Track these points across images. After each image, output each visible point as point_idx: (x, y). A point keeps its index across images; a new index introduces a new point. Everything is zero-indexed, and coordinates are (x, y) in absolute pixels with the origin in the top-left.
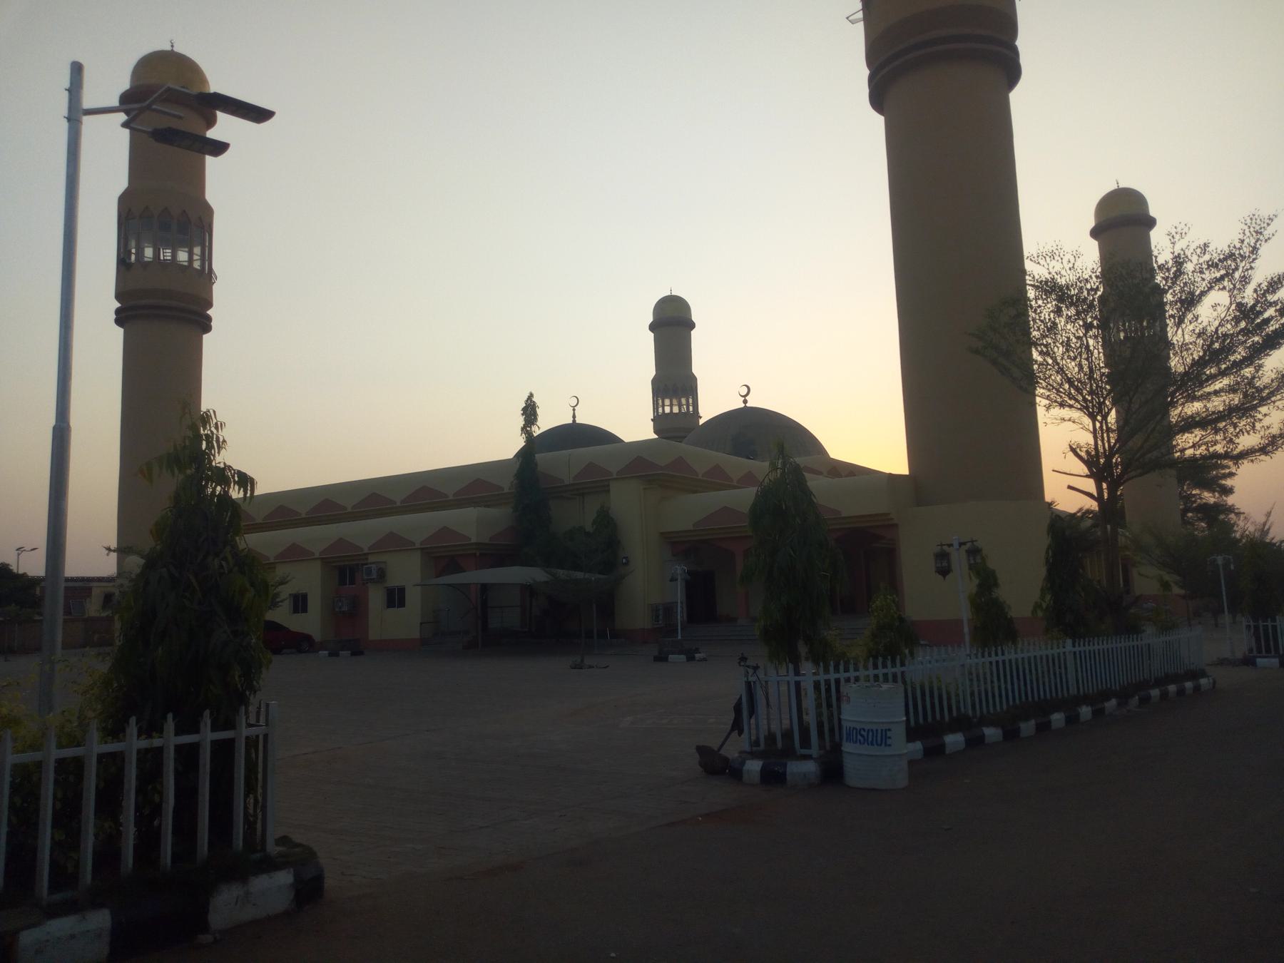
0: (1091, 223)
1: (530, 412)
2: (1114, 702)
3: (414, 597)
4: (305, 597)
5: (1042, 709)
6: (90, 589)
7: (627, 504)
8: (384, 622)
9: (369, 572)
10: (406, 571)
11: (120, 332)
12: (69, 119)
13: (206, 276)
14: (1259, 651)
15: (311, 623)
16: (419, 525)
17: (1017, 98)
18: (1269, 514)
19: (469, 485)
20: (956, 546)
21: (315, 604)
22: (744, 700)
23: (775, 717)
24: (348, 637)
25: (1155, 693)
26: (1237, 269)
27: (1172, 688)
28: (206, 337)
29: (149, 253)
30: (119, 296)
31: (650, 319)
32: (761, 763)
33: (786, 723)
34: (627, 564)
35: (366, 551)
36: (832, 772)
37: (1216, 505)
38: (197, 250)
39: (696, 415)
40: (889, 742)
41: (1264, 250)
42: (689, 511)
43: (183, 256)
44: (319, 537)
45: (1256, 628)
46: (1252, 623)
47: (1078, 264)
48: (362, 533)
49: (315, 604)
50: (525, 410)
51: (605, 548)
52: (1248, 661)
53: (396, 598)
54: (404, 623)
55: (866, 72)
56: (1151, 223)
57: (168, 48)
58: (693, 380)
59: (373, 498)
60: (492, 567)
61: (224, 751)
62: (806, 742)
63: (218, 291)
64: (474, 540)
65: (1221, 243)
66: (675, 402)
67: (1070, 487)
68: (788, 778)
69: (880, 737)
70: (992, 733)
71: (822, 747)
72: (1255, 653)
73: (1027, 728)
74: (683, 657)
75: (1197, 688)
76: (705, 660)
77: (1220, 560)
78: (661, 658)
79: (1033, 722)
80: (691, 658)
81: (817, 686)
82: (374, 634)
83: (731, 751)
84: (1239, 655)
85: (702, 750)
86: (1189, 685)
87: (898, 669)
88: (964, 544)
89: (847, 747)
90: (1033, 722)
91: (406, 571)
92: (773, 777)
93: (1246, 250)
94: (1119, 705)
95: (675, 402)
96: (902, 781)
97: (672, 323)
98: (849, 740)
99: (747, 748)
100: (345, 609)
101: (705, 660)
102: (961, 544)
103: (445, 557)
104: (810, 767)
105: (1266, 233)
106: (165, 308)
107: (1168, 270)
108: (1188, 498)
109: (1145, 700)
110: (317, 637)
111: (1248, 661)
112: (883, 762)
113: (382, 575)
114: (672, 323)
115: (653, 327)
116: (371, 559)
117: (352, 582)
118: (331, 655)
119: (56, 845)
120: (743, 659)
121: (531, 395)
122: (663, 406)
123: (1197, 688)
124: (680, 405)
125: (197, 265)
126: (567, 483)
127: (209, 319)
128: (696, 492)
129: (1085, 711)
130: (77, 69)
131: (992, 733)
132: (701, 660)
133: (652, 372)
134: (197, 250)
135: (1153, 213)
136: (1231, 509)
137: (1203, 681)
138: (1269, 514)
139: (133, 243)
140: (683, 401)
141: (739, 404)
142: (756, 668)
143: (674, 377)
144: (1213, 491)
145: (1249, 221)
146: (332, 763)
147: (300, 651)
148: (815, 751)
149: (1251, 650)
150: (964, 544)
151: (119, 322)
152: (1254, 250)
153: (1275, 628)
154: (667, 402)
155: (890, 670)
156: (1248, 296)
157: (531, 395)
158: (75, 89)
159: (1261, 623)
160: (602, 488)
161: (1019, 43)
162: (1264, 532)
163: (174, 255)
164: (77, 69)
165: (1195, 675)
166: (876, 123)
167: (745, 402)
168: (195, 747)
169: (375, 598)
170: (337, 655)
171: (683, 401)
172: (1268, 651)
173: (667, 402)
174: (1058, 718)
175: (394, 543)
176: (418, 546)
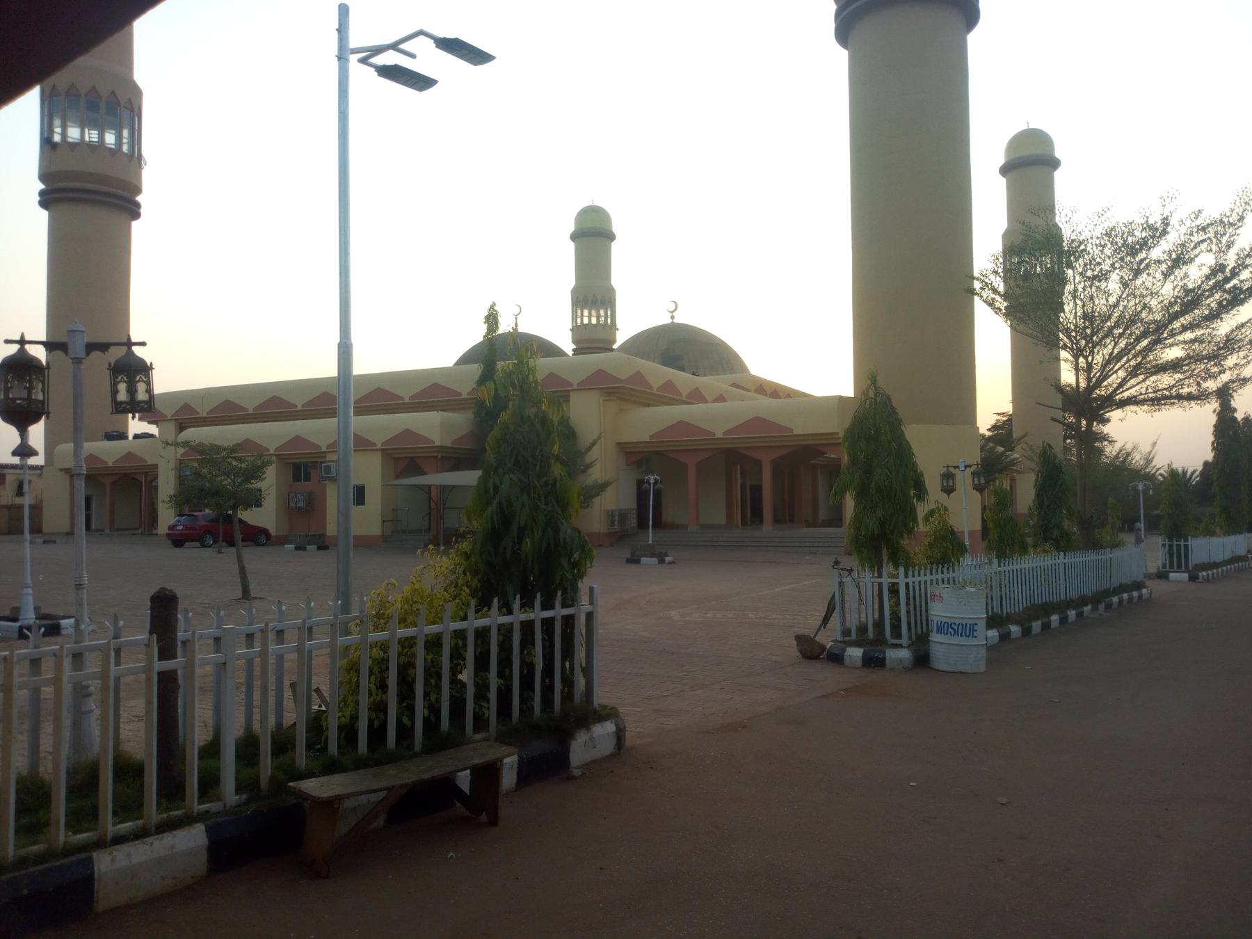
0: (1001, 160)
1: (492, 319)
2: (1089, 607)
5: (1045, 609)
7: (586, 414)
9: (328, 469)
11: (44, 215)
12: (339, 59)
13: (135, 159)
15: (264, 516)
16: (382, 426)
17: (975, 40)
18: (1154, 444)
19: (428, 391)
20: (962, 468)
24: (305, 529)
26: (1225, 234)
27: (1125, 596)
28: (135, 225)
29: (110, 139)
30: (43, 177)
32: (862, 650)
33: (863, 619)
35: (324, 449)
36: (922, 660)
38: (125, 133)
39: (613, 327)
43: (110, 139)
45: (1171, 546)
47: (1075, 219)
48: (319, 431)
50: (487, 318)
52: (1162, 576)
60: (442, 471)
61: (569, 621)
63: (149, 177)
64: (437, 443)
65: (1212, 212)
66: (594, 313)
69: (968, 630)
71: (910, 638)
73: (1036, 626)
74: (654, 560)
75: (1140, 596)
76: (673, 562)
77: (1140, 487)
78: (634, 560)
79: (1040, 622)
80: (662, 561)
81: (907, 584)
83: (827, 639)
84: (1154, 571)
85: (800, 639)
86: (1135, 594)
87: (951, 575)
88: (970, 466)
89: (935, 637)
90: (1040, 622)
91: (368, 471)
92: (873, 661)
93: (1234, 218)
95: (594, 313)
96: (982, 669)
97: (593, 235)
98: (940, 630)
99: (839, 638)
100: (301, 504)
101: (673, 562)
102: (966, 467)
103: (405, 459)
104: (904, 654)
107: (1157, 229)
109: (1109, 606)
110: (273, 531)
111: (1162, 576)
114: (593, 235)
115: (574, 237)
116: (330, 457)
117: (307, 479)
118: (297, 548)
123: (1140, 596)
124: (598, 317)
125: (125, 148)
127: (138, 205)
128: (648, 405)
129: (1072, 614)
130: (344, 11)
131: (1015, 629)
132: (670, 563)
133: (572, 282)
134: (125, 133)
135: (1058, 154)
136: (1105, 438)
137: (1144, 591)
138: (1154, 444)
139: (57, 122)
140: (602, 312)
141: (666, 320)
142: (850, 571)
143: (593, 290)
146: (673, 634)
147: (258, 544)
148: (904, 641)
149: (1164, 566)
150: (970, 466)
152: (1241, 219)
153: (1186, 547)
154: (586, 312)
155: (946, 576)
156: (1231, 259)
157: (492, 307)
158: (342, 30)
162: (1149, 461)
163: (101, 137)
164: (344, 11)
165: (1138, 586)
166: (841, 57)
167: (673, 317)
168: (552, 619)
170: (304, 549)
171: (602, 312)
172: (1179, 566)
173: (586, 312)
174: (1055, 618)
176: (379, 446)
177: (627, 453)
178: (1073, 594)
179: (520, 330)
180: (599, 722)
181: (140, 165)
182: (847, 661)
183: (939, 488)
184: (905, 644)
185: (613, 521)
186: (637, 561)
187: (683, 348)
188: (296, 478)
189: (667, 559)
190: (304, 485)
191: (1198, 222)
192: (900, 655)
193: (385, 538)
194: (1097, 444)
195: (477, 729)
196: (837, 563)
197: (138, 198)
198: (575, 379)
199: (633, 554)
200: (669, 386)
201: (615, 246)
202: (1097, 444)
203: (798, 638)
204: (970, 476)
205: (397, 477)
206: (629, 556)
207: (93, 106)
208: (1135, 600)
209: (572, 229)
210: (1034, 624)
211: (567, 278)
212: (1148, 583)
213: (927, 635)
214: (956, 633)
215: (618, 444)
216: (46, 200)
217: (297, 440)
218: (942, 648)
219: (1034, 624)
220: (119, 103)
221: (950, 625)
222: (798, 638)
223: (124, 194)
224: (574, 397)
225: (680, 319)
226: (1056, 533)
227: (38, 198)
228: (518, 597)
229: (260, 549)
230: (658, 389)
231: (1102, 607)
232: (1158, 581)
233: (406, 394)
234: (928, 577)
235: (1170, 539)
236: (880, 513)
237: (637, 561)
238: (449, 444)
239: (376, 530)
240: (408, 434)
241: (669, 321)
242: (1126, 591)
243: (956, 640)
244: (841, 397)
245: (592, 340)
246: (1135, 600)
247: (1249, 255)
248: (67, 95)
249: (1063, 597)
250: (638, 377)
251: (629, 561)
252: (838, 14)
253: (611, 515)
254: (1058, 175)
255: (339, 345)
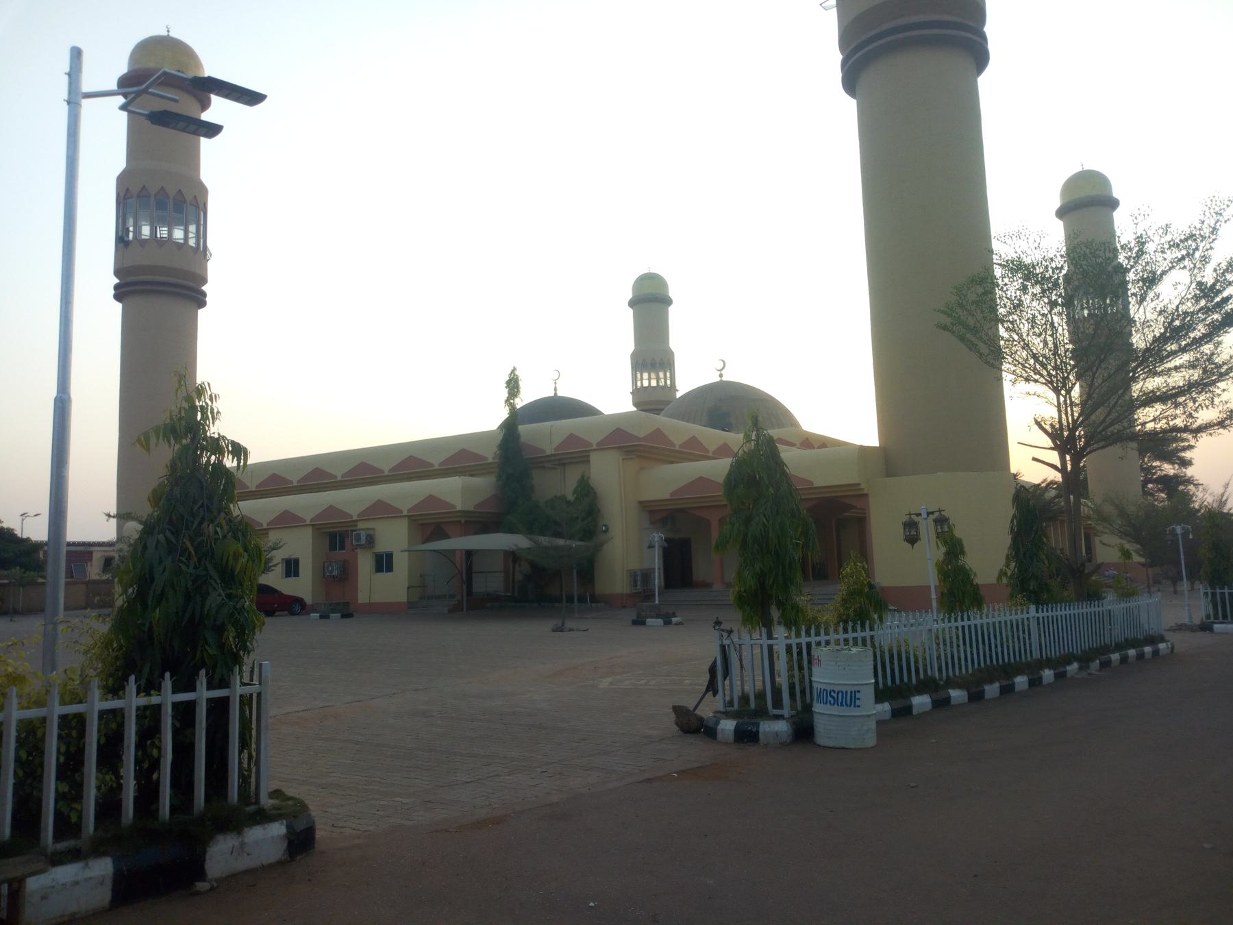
0: (1057, 203)
1: (513, 385)
2: (1075, 665)
3: (401, 563)
4: (297, 562)
6: (91, 553)
7: (606, 472)
8: (372, 586)
9: (358, 538)
10: (394, 537)
11: (118, 306)
12: (69, 102)
13: (201, 253)
14: (1216, 617)
15: (302, 587)
17: (985, 82)
19: (457, 457)
20: (924, 515)
21: (306, 568)
22: (719, 662)
23: (749, 679)
24: (339, 601)
25: (1115, 657)
26: (1197, 249)
27: (1132, 652)
29: (146, 231)
30: (117, 273)
31: (629, 295)
32: (734, 723)
33: (759, 684)
34: (606, 531)
36: (804, 732)
37: (1176, 476)
38: (192, 228)
39: (673, 388)
40: (858, 703)
41: (1223, 230)
42: (666, 481)
44: (308, 504)
45: (1214, 595)
46: (1209, 591)
48: (351, 500)
49: (306, 568)
50: (508, 383)
51: (586, 515)
52: (1206, 627)
53: (384, 563)
54: (393, 587)
55: (839, 57)
56: (1113, 204)
57: (164, 33)
58: (670, 354)
59: (362, 468)
60: (476, 533)
62: (778, 703)
64: (459, 508)
65: (1180, 228)
66: (653, 375)
67: (1034, 459)
68: (761, 736)
69: (852, 699)
70: (957, 695)
71: (793, 707)
72: (1212, 619)
73: (992, 690)
74: (660, 621)
75: (1156, 653)
76: (681, 623)
77: (1179, 530)
78: (639, 622)
79: (997, 685)
80: (667, 622)
81: (789, 649)
82: (363, 597)
83: (706, 712)
84: (1197, 622)
85: (679, 711)
86: (1148, 649)
89: (818, 708)
90: (997, 685)
91: (394, 537)
92: (746, 736)
93: (1206, 231)
94: (1080, 668)
95: (653, 375)
96: (871, 741)
97: (650, 301)
99: (722, 709)
100: (335, 573)
101: (681, 623)
102: (929, 514)
103: (431, 524)
104: (782, 727)
105: (1226, 215)
106: (161, 285)
108: (1148, 470)
109: (1105, 664)
110: (308, 600)
111: (1206, 627)
112: (853, 722)
113: (371, 541)
114: (650, 301)
115: (632, 304)
116: (361, 525)
117: (342, 547)
118: (321, 617)
119: (60, 797)
120: (718, 623)
121: (515, 369)
122: (642, 379)
124: (658, 379)
125: (192, 242)
126: (548, 453)
127: (204, 294)
128: (672, 462)
129: (1048, 675)
130: (76, 54)
131: (957, 695)
133: (630, 346)
134: (192, 228)
135: (1116, 194)
136: (1189, 481)
137: (1162, 646)
139: (131, 222)
142: (730, 632)
143: (652, 353)
144: (1173, 463)
145: (1209, 203)
146: (322, 718)
147: (292, 614)
148: (786, 711)
149: (1208, 617)
150: (932, 513)
151: (119, 296)
152: (1214, 230)
154: (646, 375)
155: (859, 634)
157: (515, 369)
158: (74, 74)
159: (1218, 591)
160: (583, 459)
161: (988, 29)
164: (76, 54)
166: (850, 106)
167: (721, 376)
169: (365, 563)
170: (327, 617)
171: (661, 374)
172: (1225, 617)
173: (646, 375)
174: (1021, 681)
175: (382, 510)
176: (405, 513)
177: (650, 512)
178: (1054, 653)
179: (559, 394)
180: (258, 823)
181: (205, 254)
182: (719, 736)
183: (902, 537)
184: (786, 716)
185: (635, 582)
186: (643, 623)
187: (732, 406)
188: (332, 547)
189: (674, 620)
190: (339, 554)
191: (1168, 238)
192: (776, 728)
193: (411, 605)
194: (1181, 488)
195: (59, 835)
196: (718, 623)
197: (204, 288)
198: (594, 440)
199: (638, 616)
200: (693, 442)
201: (672, 310)
202: (1181, 488)
203: (677, 709)
204: (932, 524)
205: (424, 542)
206: (634, 617)
207: (161, 205)
208: (1148, 656)
209: (630, 296)
210: (987, 688)
211: (628, 344)
212: (1168, 636)
213: (811, 706)
214: (836, 701)
215: (640, 503)
216: (121, 293)
217: (331, 510)
218: (828, 722)
219: (987, 688)
220: (185, 201)
221: (830, 693)
222: (677, 709)
223: (191, 284)
224: (594, 457)
225: (727, 377)
226: (1033, 585)
227: (113, 292)
228: (167, 675)
229: (295, 618)
230: (681, 446)
231: (1095, 665)
232: (1201, 634)
233: (436, 461)
234: (842, 636)
235: (1213, 587)
236: (758, 566)
237: (643, 623)
238: (471, 509)
239: (402, 596)
240: (431, 500)
241: (718, 379)
242: (1133, 647)
243: (835, 710)
244: (861, 446)
245: (649, 401)
246: (1148, 656)
247: (1226, 271)
248: (138, 196)
249: (1036, 655)
250: (658, 434)
251: (635, 623)
252: (844, 63)
253: (633, 575)
254: (671, 309)
255: (56, 400)
